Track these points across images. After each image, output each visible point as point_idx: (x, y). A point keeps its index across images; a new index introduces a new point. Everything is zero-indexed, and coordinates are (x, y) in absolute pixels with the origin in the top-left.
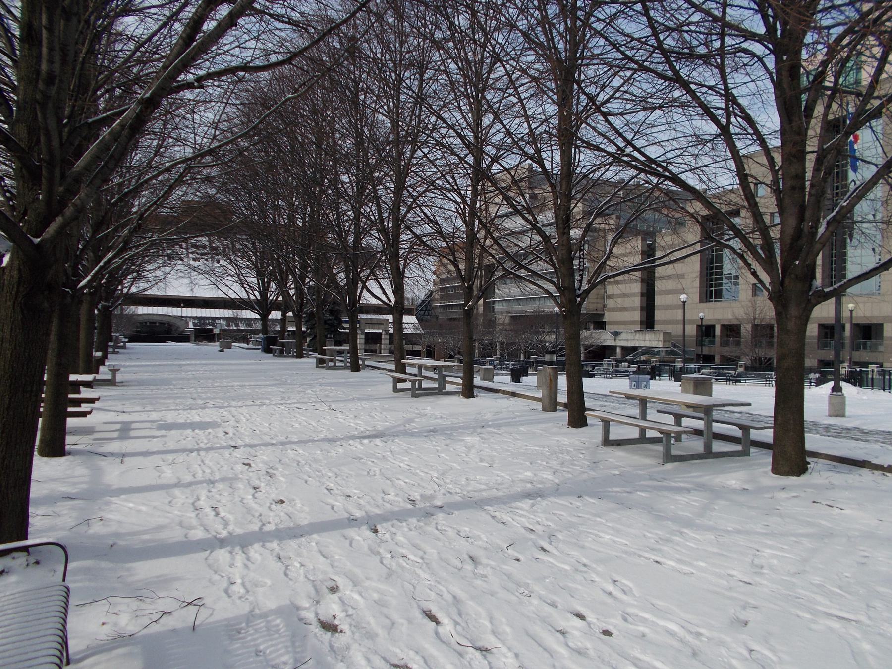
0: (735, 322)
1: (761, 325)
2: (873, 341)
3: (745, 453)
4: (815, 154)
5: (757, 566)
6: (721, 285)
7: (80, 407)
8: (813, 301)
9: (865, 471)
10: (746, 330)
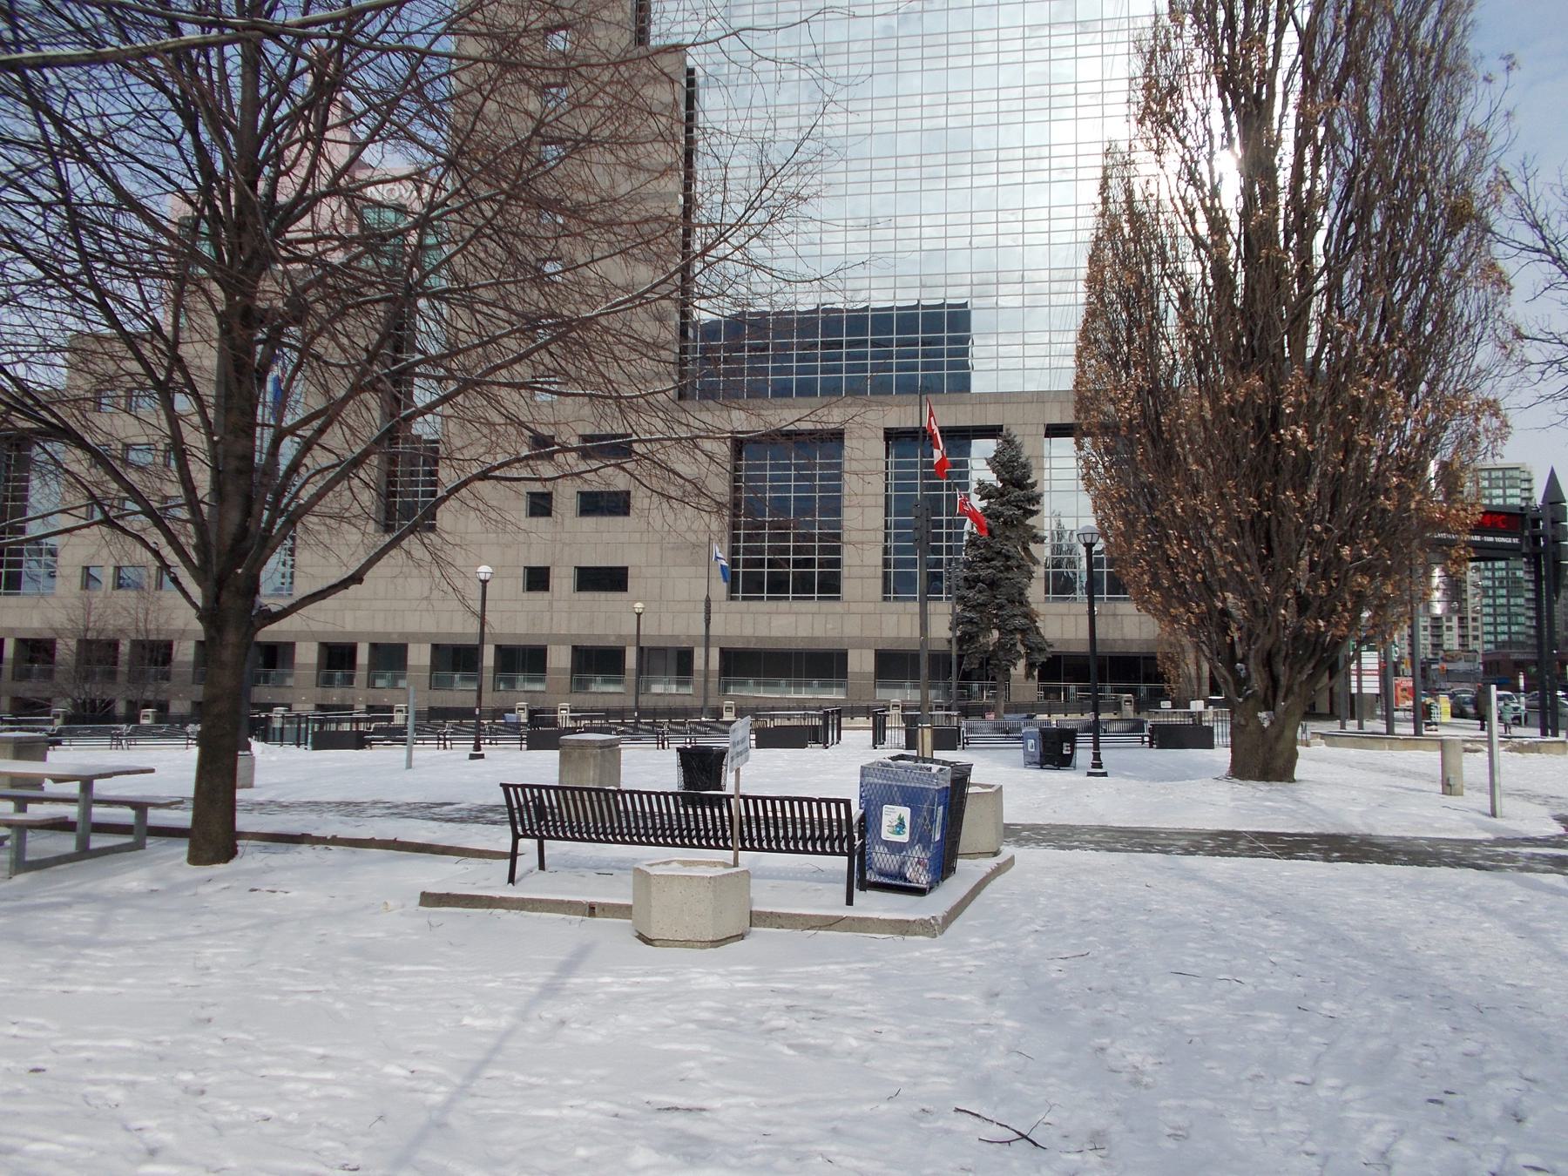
0: (48, 635)
1: (98, 642)
2: (279, 670)
3: (139, 846)
4: (320, 442)
5: (201, 969)
6: (19, 564)
7: (44, 759)
8: (257, 624)
9: (305, 847)
10: (66, 650)
